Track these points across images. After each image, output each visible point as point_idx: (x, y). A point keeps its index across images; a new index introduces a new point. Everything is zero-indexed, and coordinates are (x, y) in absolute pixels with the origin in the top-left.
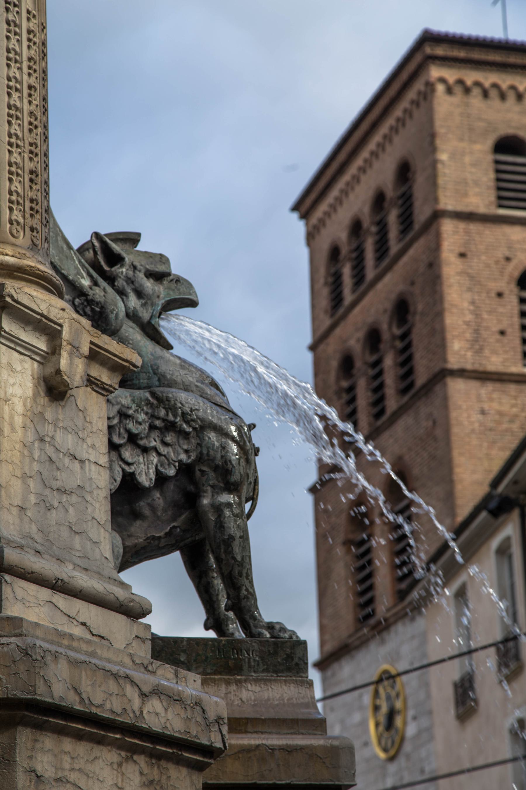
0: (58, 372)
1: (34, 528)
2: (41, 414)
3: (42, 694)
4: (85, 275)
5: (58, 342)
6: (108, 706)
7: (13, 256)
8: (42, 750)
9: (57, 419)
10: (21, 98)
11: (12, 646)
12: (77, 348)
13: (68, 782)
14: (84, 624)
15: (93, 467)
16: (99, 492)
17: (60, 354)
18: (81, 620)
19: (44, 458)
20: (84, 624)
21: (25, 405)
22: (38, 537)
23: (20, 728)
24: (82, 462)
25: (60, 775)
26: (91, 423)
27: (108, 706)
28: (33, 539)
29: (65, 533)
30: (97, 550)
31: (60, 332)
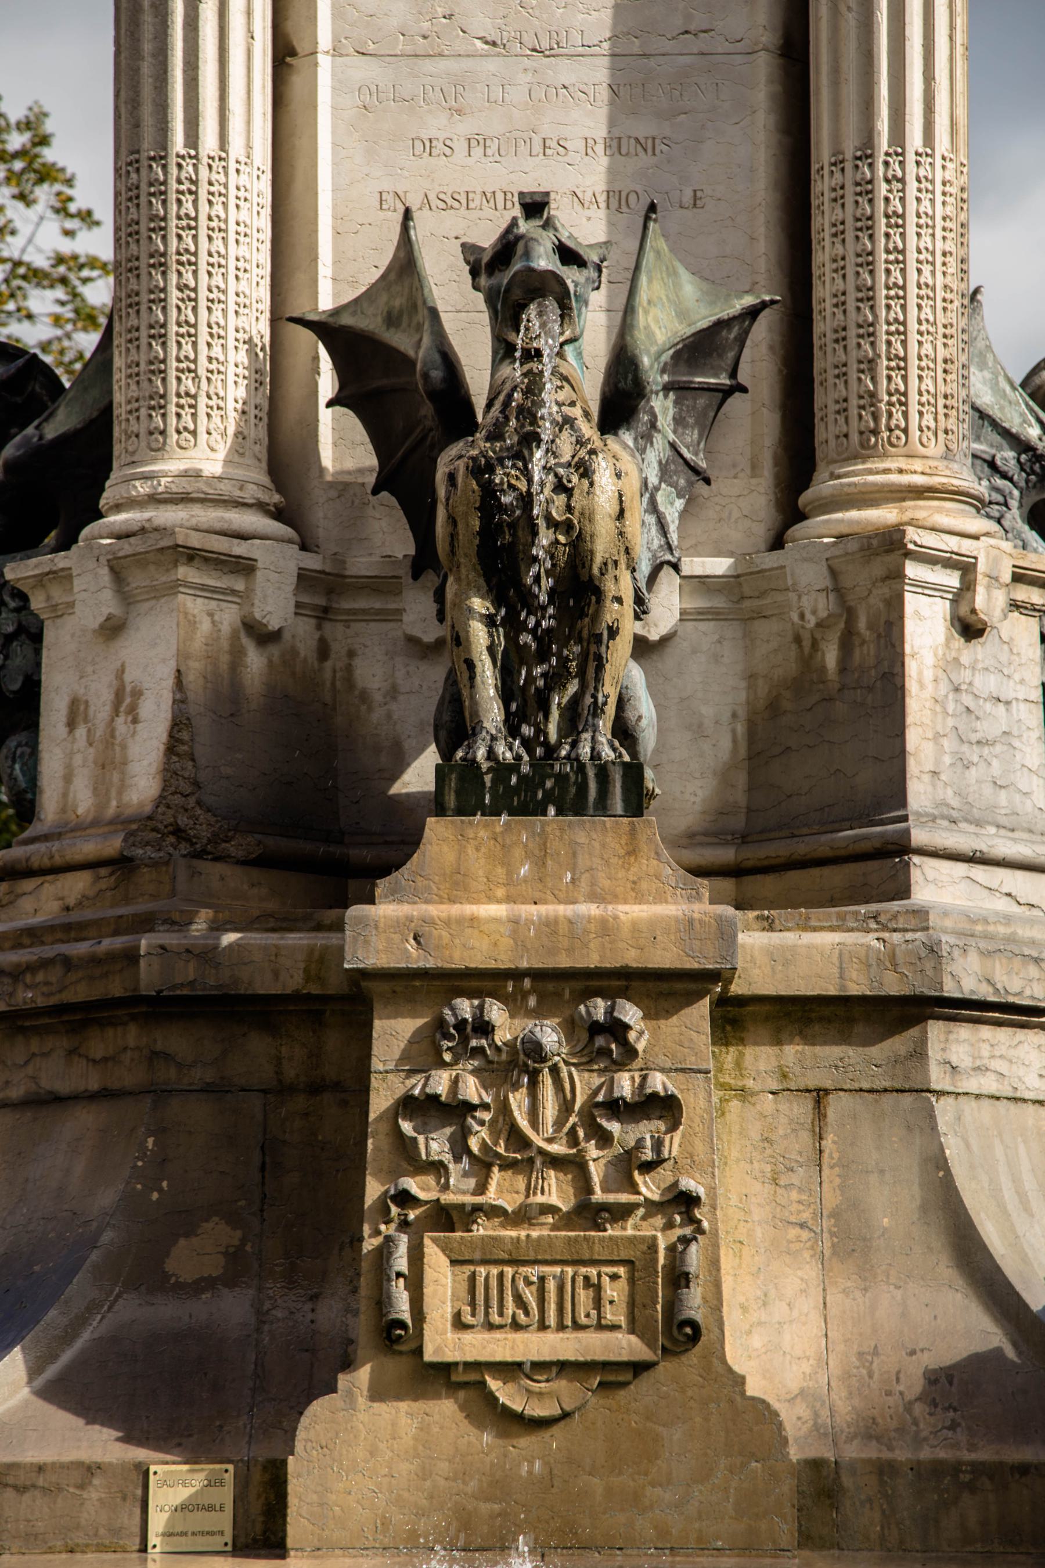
0: (974, 611)
1: (950, 792)
2: (956, 660)
3: (950, 990)
4: (1033, 421)
5: (972, 577)
6: (1028, 992)
7: (923, 473)
8: (957, 1041)
9: (976, 661)
10: (933, 273)
11: (917, 943)
12: (996, 579)
13: (987, 1069)
14: (1009, 895)
15: (1022, 706)
16: (1031, 733)
17: (974, 591)
18: (1005, 890)
19: (961, 709)
20: (1009, 895)
21: (935, 655)
22: (955, 802)
23: (930, 1022)
24: (1008, 703)
25: (978, 1063)
26: (1018, 654)
27: (1028, 992)
28: (948, 805)
29: (988, 790)
30: (1028, 803)
31: (975, 565)
